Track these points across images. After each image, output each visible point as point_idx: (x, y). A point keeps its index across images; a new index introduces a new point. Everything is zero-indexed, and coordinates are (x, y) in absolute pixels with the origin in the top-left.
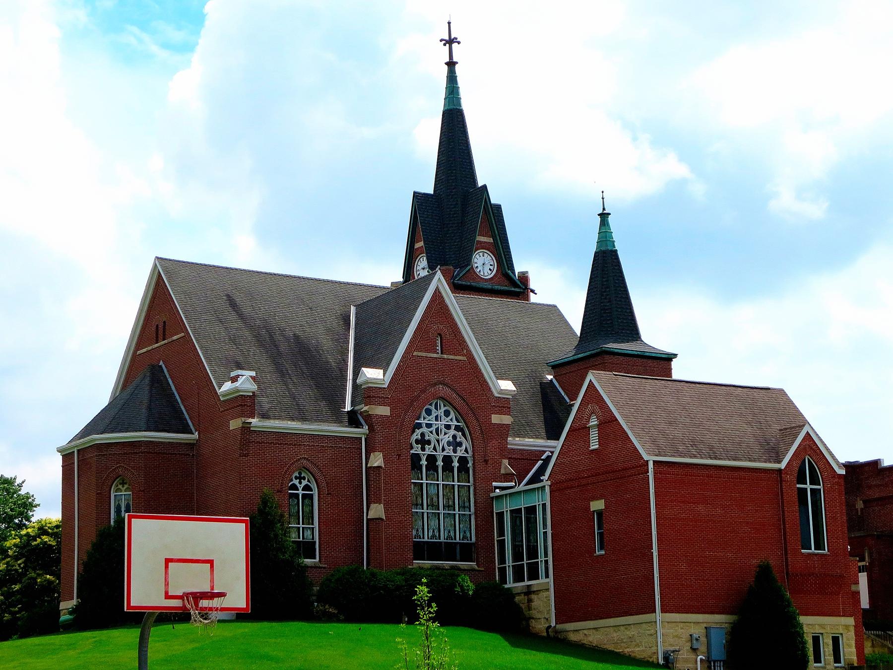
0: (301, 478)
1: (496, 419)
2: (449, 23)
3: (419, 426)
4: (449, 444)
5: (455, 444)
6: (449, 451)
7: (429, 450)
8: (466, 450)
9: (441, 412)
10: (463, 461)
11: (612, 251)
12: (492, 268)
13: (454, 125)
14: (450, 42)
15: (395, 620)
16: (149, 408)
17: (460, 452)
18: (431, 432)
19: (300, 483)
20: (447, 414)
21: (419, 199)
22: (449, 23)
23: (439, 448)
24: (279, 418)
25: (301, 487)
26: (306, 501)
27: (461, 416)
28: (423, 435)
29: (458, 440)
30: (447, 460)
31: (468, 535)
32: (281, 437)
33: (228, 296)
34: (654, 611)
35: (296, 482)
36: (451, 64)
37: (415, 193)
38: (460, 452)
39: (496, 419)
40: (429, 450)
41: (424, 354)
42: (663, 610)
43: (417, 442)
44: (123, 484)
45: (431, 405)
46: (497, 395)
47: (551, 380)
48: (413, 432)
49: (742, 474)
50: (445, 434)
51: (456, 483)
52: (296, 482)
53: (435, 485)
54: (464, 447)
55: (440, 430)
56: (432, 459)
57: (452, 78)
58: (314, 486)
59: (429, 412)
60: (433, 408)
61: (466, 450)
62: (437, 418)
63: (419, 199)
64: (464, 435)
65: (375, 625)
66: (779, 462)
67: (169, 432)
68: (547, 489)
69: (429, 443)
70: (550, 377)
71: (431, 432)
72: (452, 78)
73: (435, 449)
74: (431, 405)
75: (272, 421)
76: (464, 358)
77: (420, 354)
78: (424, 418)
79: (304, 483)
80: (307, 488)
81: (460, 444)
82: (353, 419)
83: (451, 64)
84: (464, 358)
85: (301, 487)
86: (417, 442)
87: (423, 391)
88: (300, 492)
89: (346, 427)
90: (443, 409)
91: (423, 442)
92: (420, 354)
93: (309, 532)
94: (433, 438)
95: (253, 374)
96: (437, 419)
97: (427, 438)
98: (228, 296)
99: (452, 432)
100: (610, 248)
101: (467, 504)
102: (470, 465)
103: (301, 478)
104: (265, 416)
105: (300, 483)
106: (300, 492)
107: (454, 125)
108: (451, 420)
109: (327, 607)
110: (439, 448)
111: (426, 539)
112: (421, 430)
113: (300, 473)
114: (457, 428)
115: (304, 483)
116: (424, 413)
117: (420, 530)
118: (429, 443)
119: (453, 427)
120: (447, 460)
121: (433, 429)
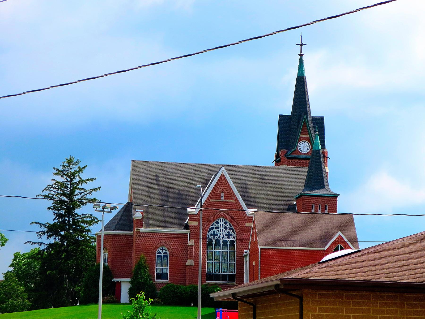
0: (162, 250)
1: (247, 225)
2: (301, 36)
3: (213, 228)
4: (226, 235)
5: (228, 235)
6: (226, 238)
7: (216, 238)
8: (234, 237)
9: (223, 223)
10: (232, 242)
11: (317, 150)
12: (308, 148)
13: (301, 82)
14: (301, 45)
15: (188, 305)
16: (119, 221)
17: (231, 238)
18: (218, 231)
19: (162, 251)
20: (226, 223)
21: (283, 119)
22: (301, 36)
23: (221, 237)
24: (154, 227)
25: (162, 253)
26: (165, 258)
27: (232, 223)
28: (214, 232)
29: (230, 233)
30: (225, 242)
31: (233, 271)
32: (154, 235)
33: (156, 175)
34: (196, 305)
35: (161, 251)
36: (301, 55)
37: (279, 115)
38: (231, 238)
39: (247, 225)
40: (216, 238)
41: (215, 200)
42: (203, 306)
43: (211, 235)
44: (107, 250)
45: (218, 220)
46: (248, 215)
47: (295, 204)
48: (209, 231)
49: (308, 252)
50: (224, 231)
51: (228, 251)
52: (161, 251)
53: (217, 251)
54: (233, 236)
55: (222, 230)
56: (217, 242)
57: (301, 62)
58: (168, 252)
59: (217, 223)
60: (219, 221)
61: (234, 237)
62: (220, 225)
63: (283, 119)
64: (233, 231)
65: (182, 307)
66: (324, 247)
67: (123, 230)
68: (249, 255)
69: (217, 235)
70: (295, 203)
71: (218, 231)
72: (301, 62)
73: (219, 237)
74: (218, 220)
75: (150, 228)
76: (234, 201)
77: (213, 200)
78: (215, 225)
79: (164, 251)
80: (165, 253)
81: (231, 235)
82: (187, 227)
83: (301, 55)
84: (234, 201)
85: (162, 253)
86: (211, 235)
87: (214, 215)
88: (162, 255)
89: (183, 229)
90: (224, 221)
91: (214, 235)
92: (213, 200)
93: (166, 270)
94: (218, 233)
95: (142, 211)
96: (220, 226)
97: (216, 233)
98: (156, 175)
99: (228, 230)
100: (316, 149)
101: (233, 259)
102: (235, 243)
103: (162, 250)
104: (148, 226)
105: (162, 251)
106: (162, 255)
107: (301, 82)
108: (228, 226)
109: (5, 306)
110: (221, 237)
111: (213, 273)
112: (213, 230)
113: (162, 248)
114: (230, 229)
115: (164, 251)
116: (215, 223)
117: (211, 269)
118: (217, 235)
119: (228, 229)
120: (225, 242)
121: (219, 229)
